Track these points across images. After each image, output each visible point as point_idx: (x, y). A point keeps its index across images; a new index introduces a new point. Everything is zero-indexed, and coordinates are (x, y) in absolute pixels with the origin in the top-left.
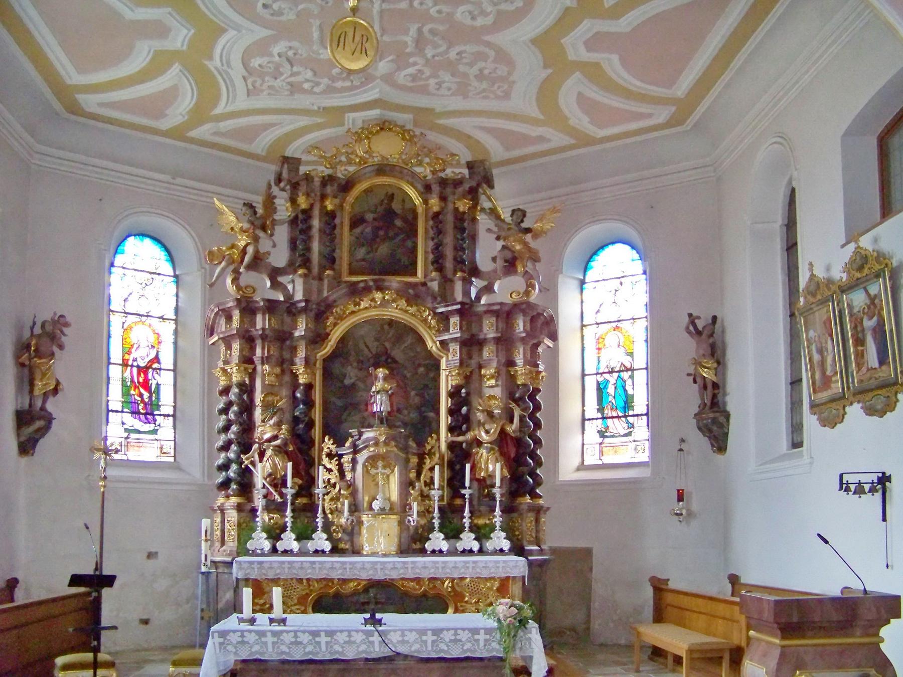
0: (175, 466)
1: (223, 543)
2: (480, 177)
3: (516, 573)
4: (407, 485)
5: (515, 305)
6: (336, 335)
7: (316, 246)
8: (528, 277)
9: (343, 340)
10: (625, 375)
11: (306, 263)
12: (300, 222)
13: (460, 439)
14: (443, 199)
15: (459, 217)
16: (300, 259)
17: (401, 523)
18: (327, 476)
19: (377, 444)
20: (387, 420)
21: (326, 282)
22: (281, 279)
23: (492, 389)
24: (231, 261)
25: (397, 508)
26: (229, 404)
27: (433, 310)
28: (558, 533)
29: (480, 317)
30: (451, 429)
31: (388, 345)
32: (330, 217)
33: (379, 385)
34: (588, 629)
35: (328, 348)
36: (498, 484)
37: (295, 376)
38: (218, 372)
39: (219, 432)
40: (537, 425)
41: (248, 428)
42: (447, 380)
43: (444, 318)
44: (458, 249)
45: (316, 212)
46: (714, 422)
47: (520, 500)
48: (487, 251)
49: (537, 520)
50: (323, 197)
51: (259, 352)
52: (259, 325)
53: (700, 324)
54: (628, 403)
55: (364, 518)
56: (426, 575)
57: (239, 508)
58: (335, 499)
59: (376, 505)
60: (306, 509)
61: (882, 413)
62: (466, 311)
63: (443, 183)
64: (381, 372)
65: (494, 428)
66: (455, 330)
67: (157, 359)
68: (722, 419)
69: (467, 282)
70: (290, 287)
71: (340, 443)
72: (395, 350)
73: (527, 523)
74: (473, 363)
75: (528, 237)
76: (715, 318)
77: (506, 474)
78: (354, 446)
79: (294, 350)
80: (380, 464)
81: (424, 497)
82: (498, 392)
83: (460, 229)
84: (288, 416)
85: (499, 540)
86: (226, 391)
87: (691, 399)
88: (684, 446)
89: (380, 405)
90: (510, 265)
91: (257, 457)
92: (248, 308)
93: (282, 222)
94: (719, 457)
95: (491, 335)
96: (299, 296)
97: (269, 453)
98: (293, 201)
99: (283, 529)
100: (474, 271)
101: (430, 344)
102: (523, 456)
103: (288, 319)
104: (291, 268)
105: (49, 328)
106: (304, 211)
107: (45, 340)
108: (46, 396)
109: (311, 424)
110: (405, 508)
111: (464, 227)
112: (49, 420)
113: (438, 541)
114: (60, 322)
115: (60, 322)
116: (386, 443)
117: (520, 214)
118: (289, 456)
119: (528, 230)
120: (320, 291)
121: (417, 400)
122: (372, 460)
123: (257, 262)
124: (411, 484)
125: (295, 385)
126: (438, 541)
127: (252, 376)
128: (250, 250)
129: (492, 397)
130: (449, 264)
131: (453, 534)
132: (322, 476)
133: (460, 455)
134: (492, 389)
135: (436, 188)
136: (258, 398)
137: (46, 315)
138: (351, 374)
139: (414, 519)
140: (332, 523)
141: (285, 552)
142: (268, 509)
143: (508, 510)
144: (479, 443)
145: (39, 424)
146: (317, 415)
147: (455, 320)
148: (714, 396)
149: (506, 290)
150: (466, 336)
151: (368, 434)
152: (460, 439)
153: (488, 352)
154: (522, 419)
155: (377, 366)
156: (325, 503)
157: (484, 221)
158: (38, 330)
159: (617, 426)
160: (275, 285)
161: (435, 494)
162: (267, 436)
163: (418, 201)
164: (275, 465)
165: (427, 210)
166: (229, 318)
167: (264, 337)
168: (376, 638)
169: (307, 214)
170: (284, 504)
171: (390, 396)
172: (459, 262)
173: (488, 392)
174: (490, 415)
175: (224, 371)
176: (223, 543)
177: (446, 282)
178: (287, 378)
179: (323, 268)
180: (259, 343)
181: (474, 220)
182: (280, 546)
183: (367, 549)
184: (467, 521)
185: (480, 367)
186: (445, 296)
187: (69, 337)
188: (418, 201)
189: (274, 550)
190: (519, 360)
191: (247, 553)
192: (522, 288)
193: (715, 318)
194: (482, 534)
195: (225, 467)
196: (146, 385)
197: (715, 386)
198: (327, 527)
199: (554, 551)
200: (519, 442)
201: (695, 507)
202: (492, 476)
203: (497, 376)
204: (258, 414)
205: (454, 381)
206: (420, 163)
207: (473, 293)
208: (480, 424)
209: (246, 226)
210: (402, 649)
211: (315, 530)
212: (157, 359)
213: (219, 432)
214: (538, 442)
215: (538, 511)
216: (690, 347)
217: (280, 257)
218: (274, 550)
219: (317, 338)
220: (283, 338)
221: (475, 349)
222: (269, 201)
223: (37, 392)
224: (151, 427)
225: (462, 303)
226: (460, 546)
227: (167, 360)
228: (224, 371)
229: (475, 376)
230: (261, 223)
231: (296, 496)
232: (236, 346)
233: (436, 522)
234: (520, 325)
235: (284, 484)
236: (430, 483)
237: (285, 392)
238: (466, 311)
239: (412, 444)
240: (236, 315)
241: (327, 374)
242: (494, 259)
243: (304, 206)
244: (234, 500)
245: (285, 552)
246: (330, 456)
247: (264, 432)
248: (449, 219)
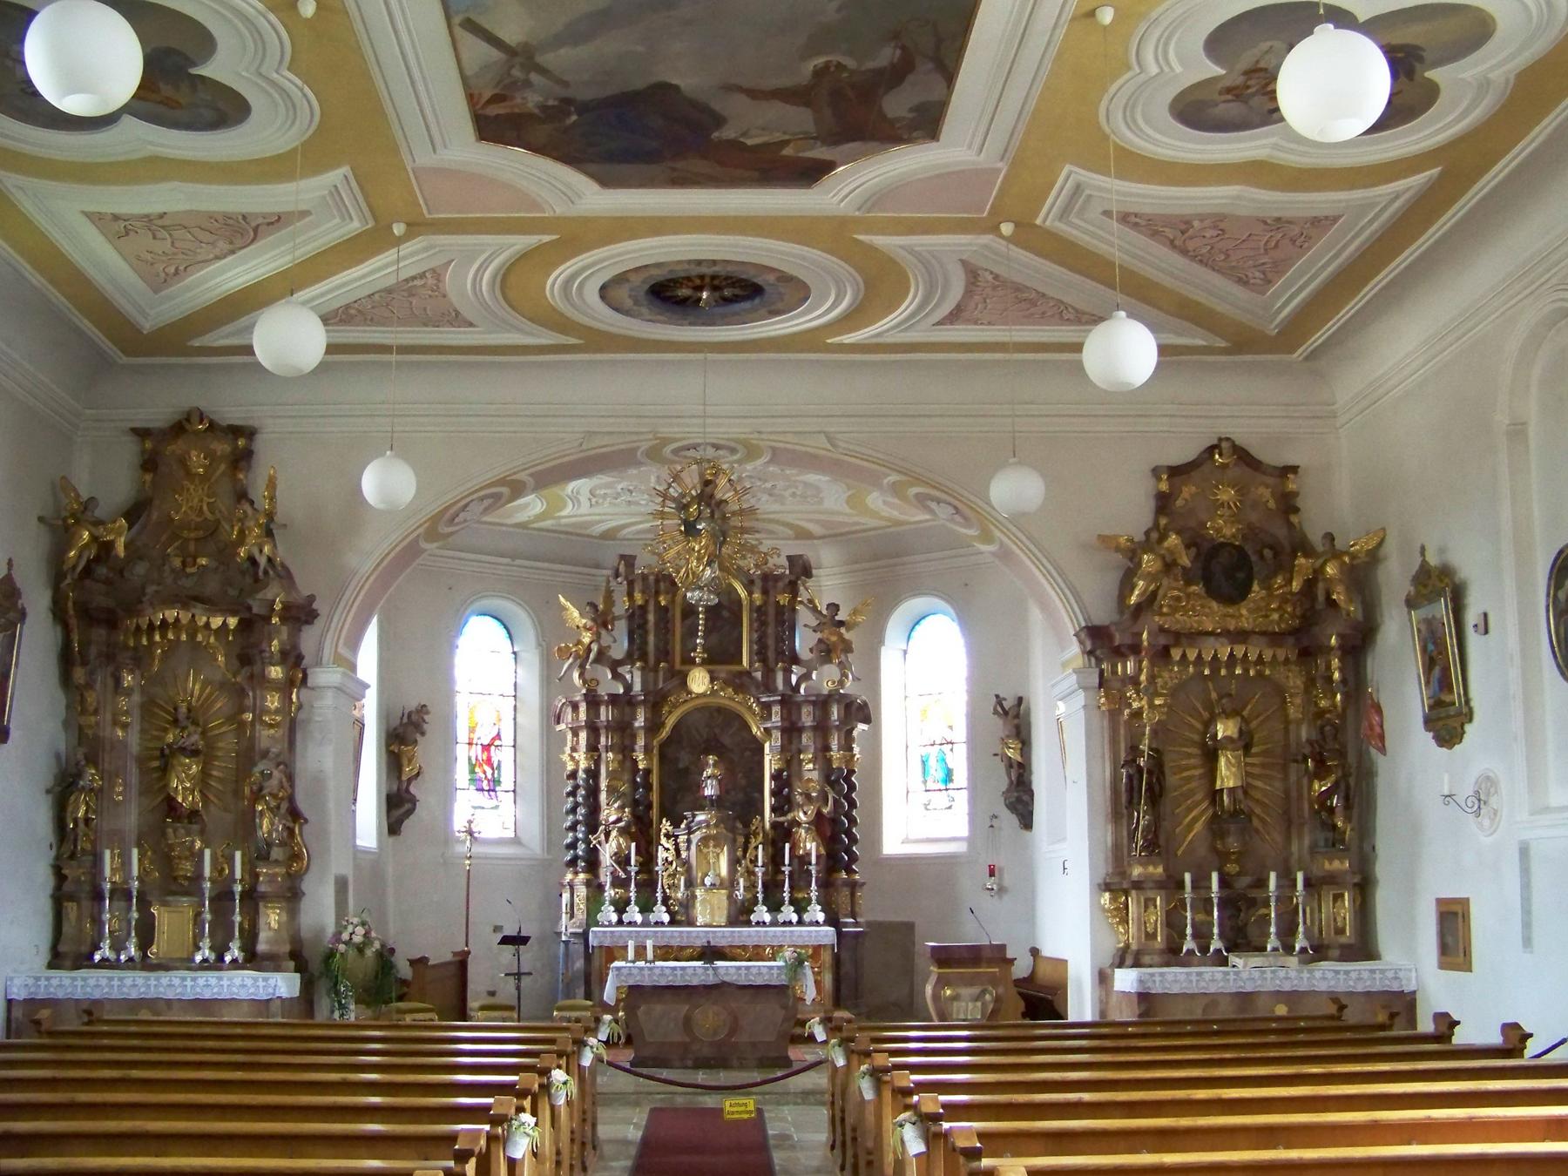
0: (516, 841)
1: (572, 916)
2: (801, 569)
3: (826, 941)
4: (734, 862)
5: (830, 696)
6: (670, 722)
7: (651, 638)
8: (843, 666)
9: (676, 727)
10: (947, 748)
11: (643, 657)
12: (636, 620)
13: (782, 819)
14: (765, 592)
15: (780, 610)
16: (637, 652)
17: (730, 897)
18: (665, 855)
19: (708, 826)
20: (717, 803)
21: (661, 674)
22: (620, 670)
23: (810, 770)
24: (577, 657)
25: (727, 883)
26: (576, 787)
27: (757, 700)
28: (874, 908)
29: (799, 706)
30: (773, 809)
31: (717, 731)
32: (663, 612)
33: (709, 771)
34: (911, 1004)
35: (665, 733)
36: (814, 861)
37: (635, 762)
38: (565, 757)
39: (568, 813)
40: (852, 804)
41: (594, 809)
42: (770, 763)
43: (766, 707)
44: (779, 640)
45: (651, 608)
46: (1020, 798)
47: (836, 875)
48: (803, 642)
49: (853, 895)
50: (657, 593)
51: (603, 740)
52: (603, 718)
53: (1007, 705)
54: (949, 776)
55: (698, 893)
56: (749, 943)
57: (588, 884)
58: (673, 876)
59: (708, 881)
60: (648, 885)
61: (1451, 747)
62: (789, 702)
63: (766, 577)
64: (711, 759)
65: (811, 810)
66: (776, 718)
67: (498, 736)
68: (1025, 798)
69: (788, 672)
70: (628, 677)
71: (676, 825)
72: (720, 734)
73: (843, 896)
74: (794, 747)
75: (843, 630)
76: (1020, 700)
77: (823, 852)
78: (688, 827)
79: (634, 737)
80: (711, 844)
81: (750, 873)
82: (815, 775)
83: (780, 622)
84: (629, 799)
85: (816, 913)
86: (573, 775)
87: (1001, 781)
88: (995, 822)
89: (710, 790)
90: (826, 652)
91: (603, 837)
92: (593, 701)
93: (619, 618)
94: (1026, 833)
95: (809, 723)
96: (637, 687)
97: (614, 833)
98: (630, 595)
99: (628, 902)
100: (795, 659)
101: (754, 730)
102: (842, 831)
103: (627, 709)
104: (629, 658)
105: (414, 718)
106: (641, 607)
107: (411, 728)
108: (409, 781)
109: (649, 806)
110: (732, 884)
111: (785, 620)
112: (413, 801)
113: (762, 913)
114: (423, 709)
115: (423, 709)
116: (716, 825)
117: (834, 608)
118: (633, 837)
119: (841, 623)
120: (656, 682)
121: (743, 782)
122: (705, 840)
123: (601, 657)
124: (738, 862)
125: (635, 770)
126: (762, 913)
127: (597, 763)
128: (595, 647)
129: (810, 780)
130: (771, 654)
131: (775, 908)
132: (661, 854)
133: (783, 833)
134: (810, 770)
135: (759, 583)
136: (603, 784)
137: (413, 705)
138: (685, 759)
139: (740, 893)
140: (669, 898)
141: (630, 924)
142: (614, 885)
143: (826, 885)
144: (799, 824)
145: (407, 806)
146: (655, 797)
147: (776, 709)
148: (1020, 776)
149: (825, 679)
150: (787, 724)
151: (701, 817)
152: (782, 819)
153: (806, 739)
154: (836, 801)
155: (707, 752)
156: (663, 880)
157: (804, 616)
158: (405, 720)
159: (940, 799)
160: (617, 676)
161: (759, 871)
162: (612, 818)
163: (742, 593)
164: (619, 845)
165: (751, 602)
166: (575, 707)
167: (607, 728)
168: (710, 972)
169: (643, 609)
170: (628, 879)
171: (720, 782)
172: (780, 654)
173: (807, 776)
174: (808, 797)
175: (573, 758)
176: (572, 916)
177: (769, 672)
178: (628, 764)
179: (658, 662)
180: (603, 732)
181: (794, 610)
182: (625, 918)
183: (700, 921)
184: (786, 895)
185: (800, 752)
186: (768, 686)
187: (432, 723)
188: (742, 593)
189: (620, 922)
190: (834, 745)
191: (597, 924)
192: (837, 677)
193: (1020, 700)
194: (800, 907)
195: (573, 846)
196: (489, 761)
197: (1020, 765)
198: (665, 901)
199: (869, 924)
200: (834, 821)
201: (1007, 882)
202: (809, 854)
203: (814, 760)
204: (603, 796)
205: (775, 767)
206: (744, 557)
207: (794, 679)
208: (801, 806)
209: (590, 624)
210: (726, 979)
211: (783, 904)
212: (498, 736)
213: (568, 813)
214: (853, 821)
215: (854, 886)
216: (998, 726)
217: (620, 649)
218: (620, 922)
219: (653, 727)
220: (622, 729)
221: (795, 734)
222: (609, 596)
223: (404, 778)
224: (494, 803)
225: (783, 695)
226: (781, 918)
227: (507, 738)
228: (573, 758)
229: (795, 762)
230: (602, 621)
231: (637, 873)
232: (583, 735)
233: (760, 896)
234: (835, 713)
235: (628, 858)
236: (754, 861)
237: (626, 777)
238: (789, 702)
239: (739, 825)
240: (583, 708)
241: (663, 757)
242: (811, 650)
243: (640, 602)
244: (582, 876)
245: (630, 924)
246: (668, 836)
247: (608, 815)
248: (771, 611)
